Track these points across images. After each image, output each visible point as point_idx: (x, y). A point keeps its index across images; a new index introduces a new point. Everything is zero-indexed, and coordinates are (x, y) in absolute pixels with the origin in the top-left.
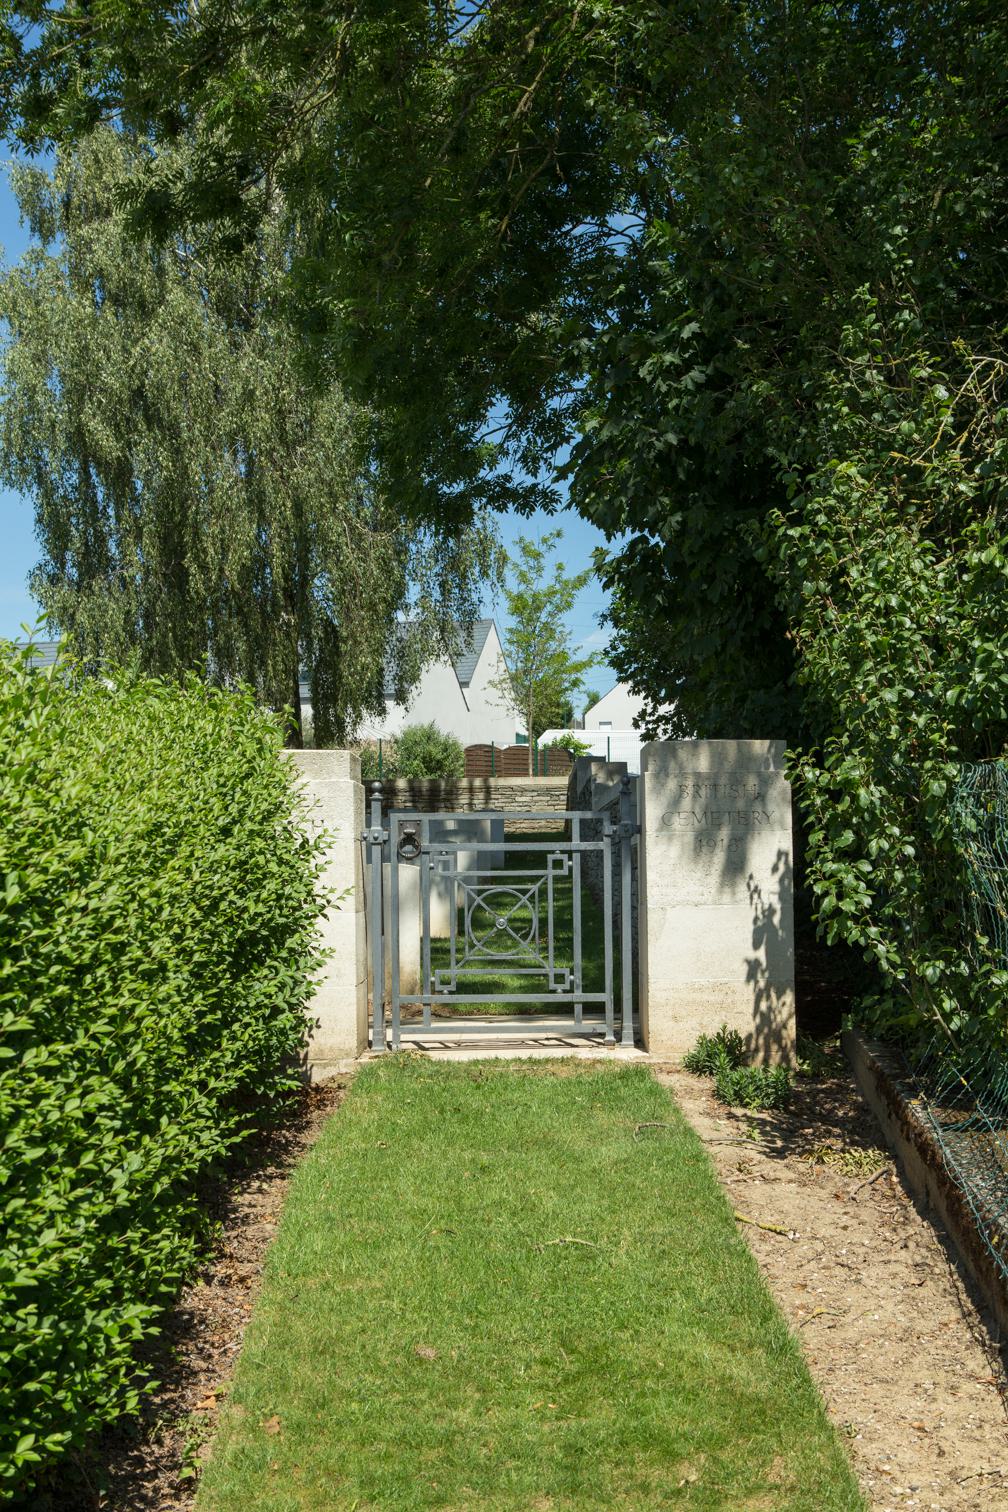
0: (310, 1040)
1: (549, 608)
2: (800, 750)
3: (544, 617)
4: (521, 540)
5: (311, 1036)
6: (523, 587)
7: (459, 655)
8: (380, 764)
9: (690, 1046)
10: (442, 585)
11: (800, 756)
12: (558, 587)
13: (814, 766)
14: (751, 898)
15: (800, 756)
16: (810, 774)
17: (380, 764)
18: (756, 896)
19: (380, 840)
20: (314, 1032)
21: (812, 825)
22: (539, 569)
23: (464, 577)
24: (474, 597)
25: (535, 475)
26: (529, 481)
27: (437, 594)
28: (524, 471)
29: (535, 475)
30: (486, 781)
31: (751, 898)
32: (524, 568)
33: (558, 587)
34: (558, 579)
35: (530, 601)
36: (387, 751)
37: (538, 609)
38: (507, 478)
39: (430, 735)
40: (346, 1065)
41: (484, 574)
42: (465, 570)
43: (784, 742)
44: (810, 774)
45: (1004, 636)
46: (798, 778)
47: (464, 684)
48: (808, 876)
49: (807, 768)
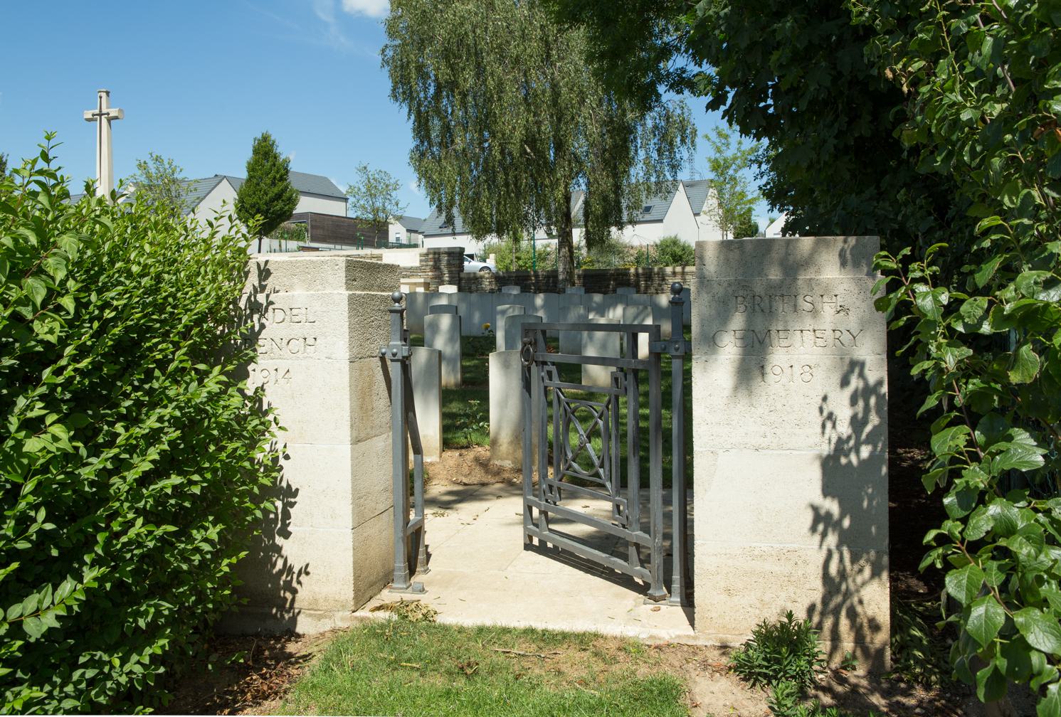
0: (298, 587)
1: (734, 166)
2: (907, 251)
3: (731, 172)
4: (717, 128)
5: (299, 583)
6: (718, 155)
7: (669, 192)
8: (647, 258)
9: (741, 634)
10: (659, 150)
11: (906, 261)
12: (739, 154)
13: (935, 282)
14: (824, 426)
15: (906, 261)
16: (928, 299)
17: (647, 258)
18: (829, 425)
19: (399, 357)
20: (303, 578)
21: (936, 412)
22: (728, 145)
23: (671, 144)
24: (678, 156)
25: (700, 66)
26: (696, 69)
27: (655, 155)
28: (693, 64)
29: (700, 66)
30: (683, 269)
31: (824, 426)
32: (719, 144)
33: (739, 154)
34: (738, 149)
35: (722, 163)
36: (652, 251)
37: (728, 167)
38: (683, 70)
39: (675, 242)
40: (342, 619)
41: (683, 141)
42: (672, 141)
43: (873, 241)
44: (928, 299)
45: (1058, 147)
46: (905, 307)
47: (696, 214)
48: (929, 548)
49: (921, 288)
